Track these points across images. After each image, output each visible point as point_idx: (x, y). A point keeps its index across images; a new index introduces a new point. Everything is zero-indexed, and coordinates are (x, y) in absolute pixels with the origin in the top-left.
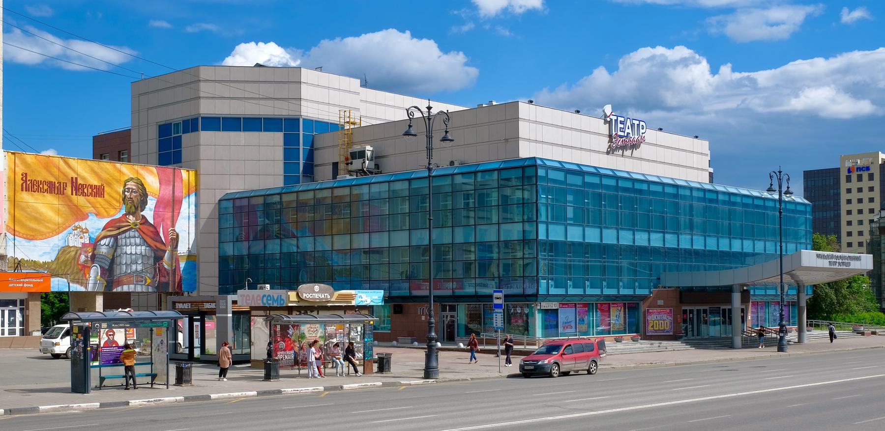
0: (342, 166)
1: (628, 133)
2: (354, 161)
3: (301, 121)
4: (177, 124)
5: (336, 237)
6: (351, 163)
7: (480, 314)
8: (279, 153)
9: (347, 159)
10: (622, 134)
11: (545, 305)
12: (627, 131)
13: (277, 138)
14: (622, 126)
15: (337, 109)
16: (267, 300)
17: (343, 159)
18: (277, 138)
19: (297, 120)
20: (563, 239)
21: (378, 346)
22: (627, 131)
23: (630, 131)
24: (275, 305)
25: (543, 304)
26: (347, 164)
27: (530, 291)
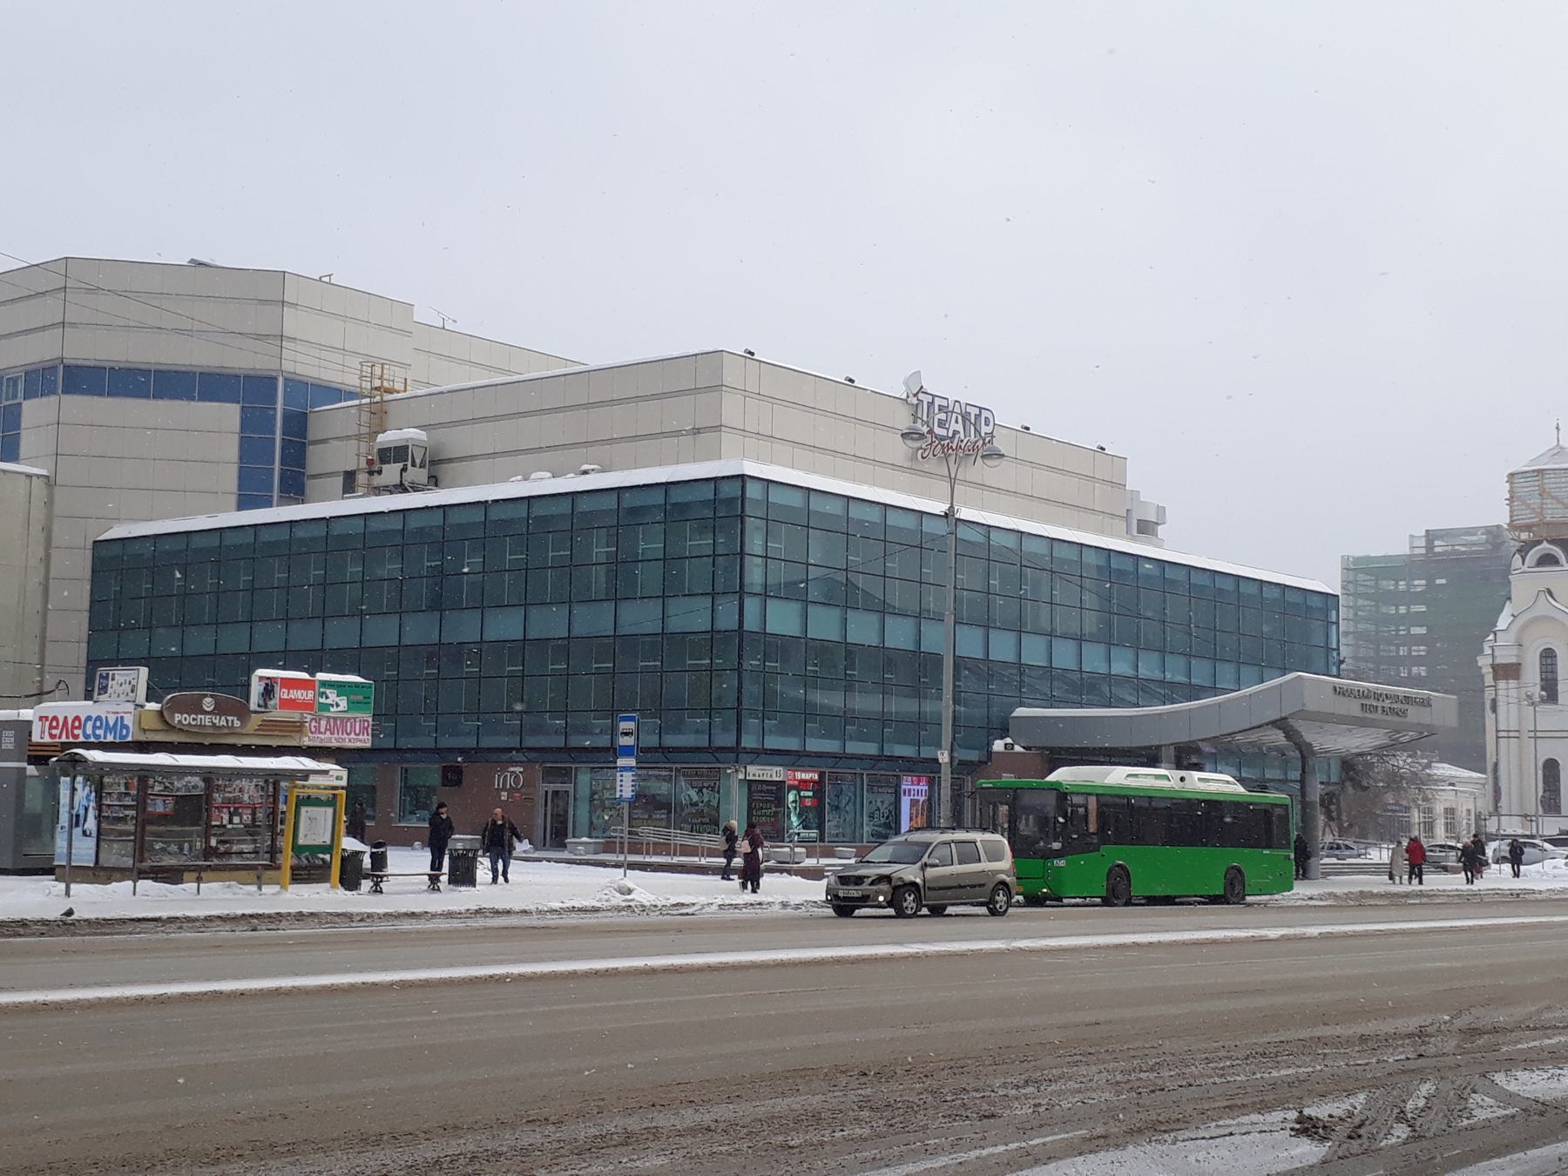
0: (362, 478)
1: (955, 432)
2: (385, 467)
3: (281, 379)
4: (15, 381)
5: (487, 612)
6: (380, 472)
7: (870, 790)
8: (230, 449)
9: (370, 462)
10: (942, 432)
11: (755, 772)
12: (954, 427)
13: (229, 415)
14: (943, 416)
15: (354, 362)
16: (95, 727)
17: (363, 464)
18: (229, 415)
19: (272, 380)
20: (874, 641)
21: (1002, 872)
22: (954, 427)
23: (960, 427)
24: (110, 738)
25: (751, 769)
26: (371, 473)
27: (725, 739)
